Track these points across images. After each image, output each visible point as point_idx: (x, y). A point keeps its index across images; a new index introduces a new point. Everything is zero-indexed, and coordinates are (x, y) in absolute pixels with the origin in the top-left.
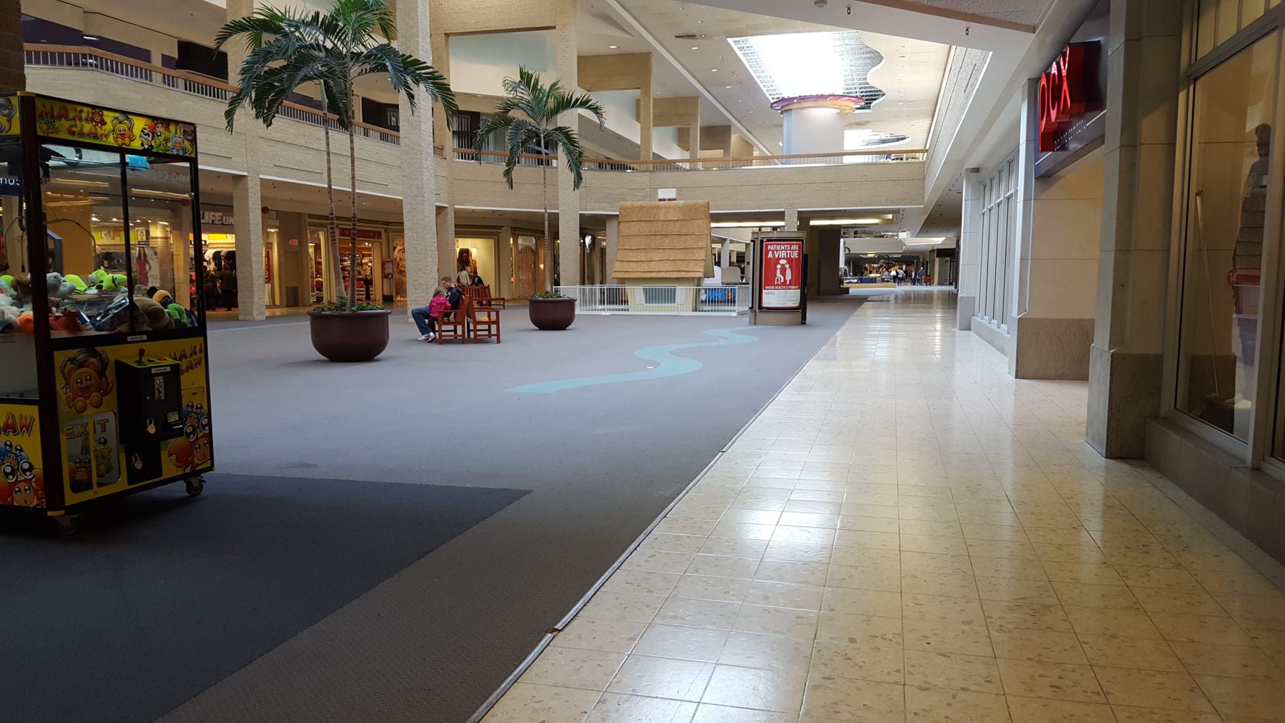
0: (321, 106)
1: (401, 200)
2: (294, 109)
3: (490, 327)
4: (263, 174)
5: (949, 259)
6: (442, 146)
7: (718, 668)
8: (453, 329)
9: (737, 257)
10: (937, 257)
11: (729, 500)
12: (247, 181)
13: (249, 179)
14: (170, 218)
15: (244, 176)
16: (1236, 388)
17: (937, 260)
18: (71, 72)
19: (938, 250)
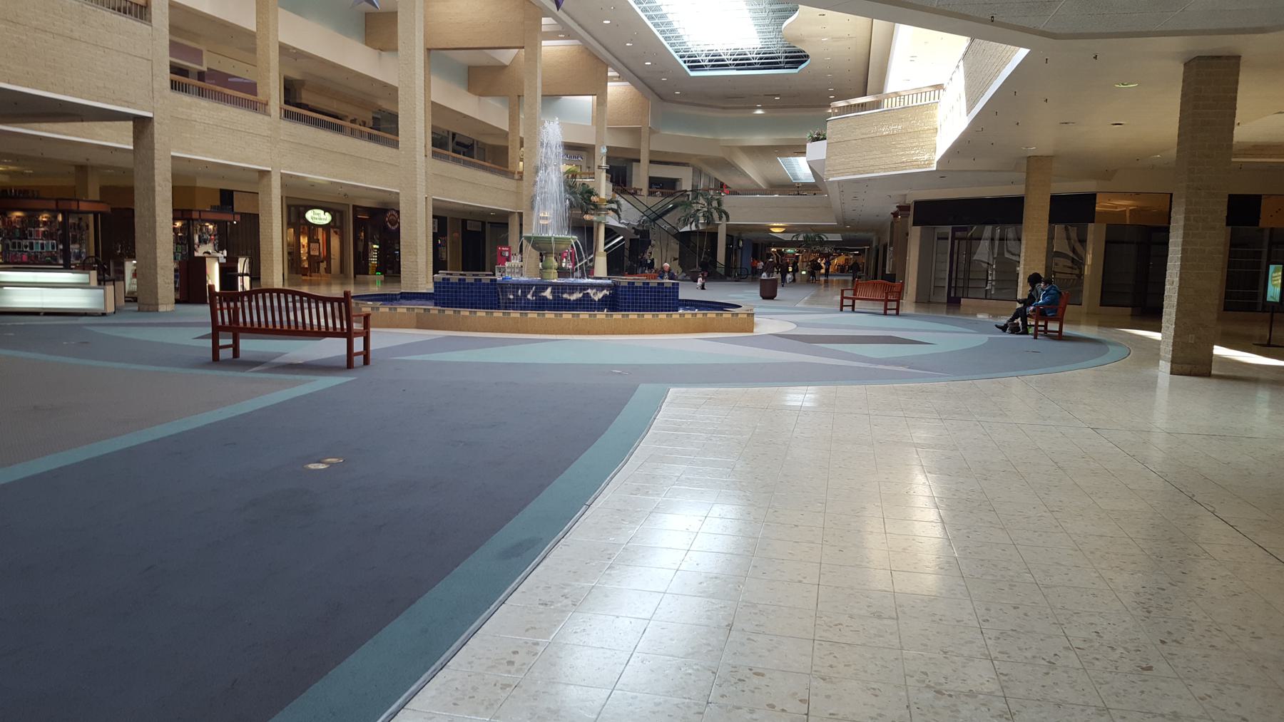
0: (251, 88)
1: (398, 194)
2: (209, 90)
3: (854, 302)
4: (284, 170)
5: (948, 229)
6: (267, 102)
7: (649, 617)
8: (851, 304)
9: (433, 209)
10: (914, 224)
11: (665, 488)
12: (271, 175)
13: (273, 173)
14: (1132, 315)
15: (269, 172)
16: (1213, 367)
17: (915, 233)
18: (177, 95)
19: (918, 204)
